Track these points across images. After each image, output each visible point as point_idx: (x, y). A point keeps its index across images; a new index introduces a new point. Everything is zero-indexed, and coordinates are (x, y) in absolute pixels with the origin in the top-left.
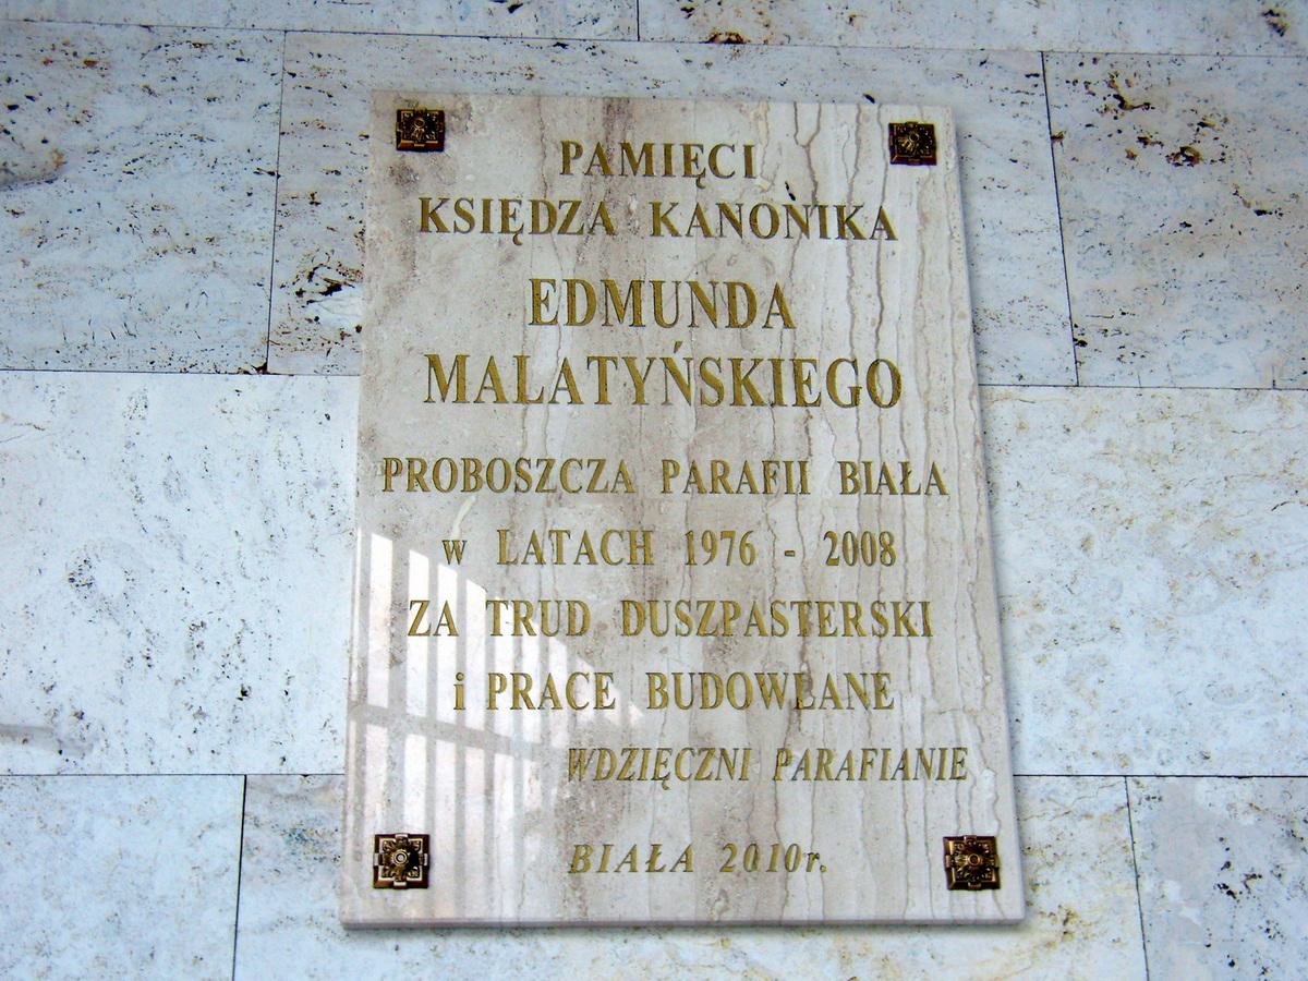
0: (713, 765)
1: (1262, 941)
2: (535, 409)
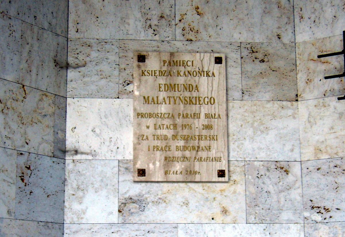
0: (185, 159)
1: (262, 185)
2: (160, 105)
